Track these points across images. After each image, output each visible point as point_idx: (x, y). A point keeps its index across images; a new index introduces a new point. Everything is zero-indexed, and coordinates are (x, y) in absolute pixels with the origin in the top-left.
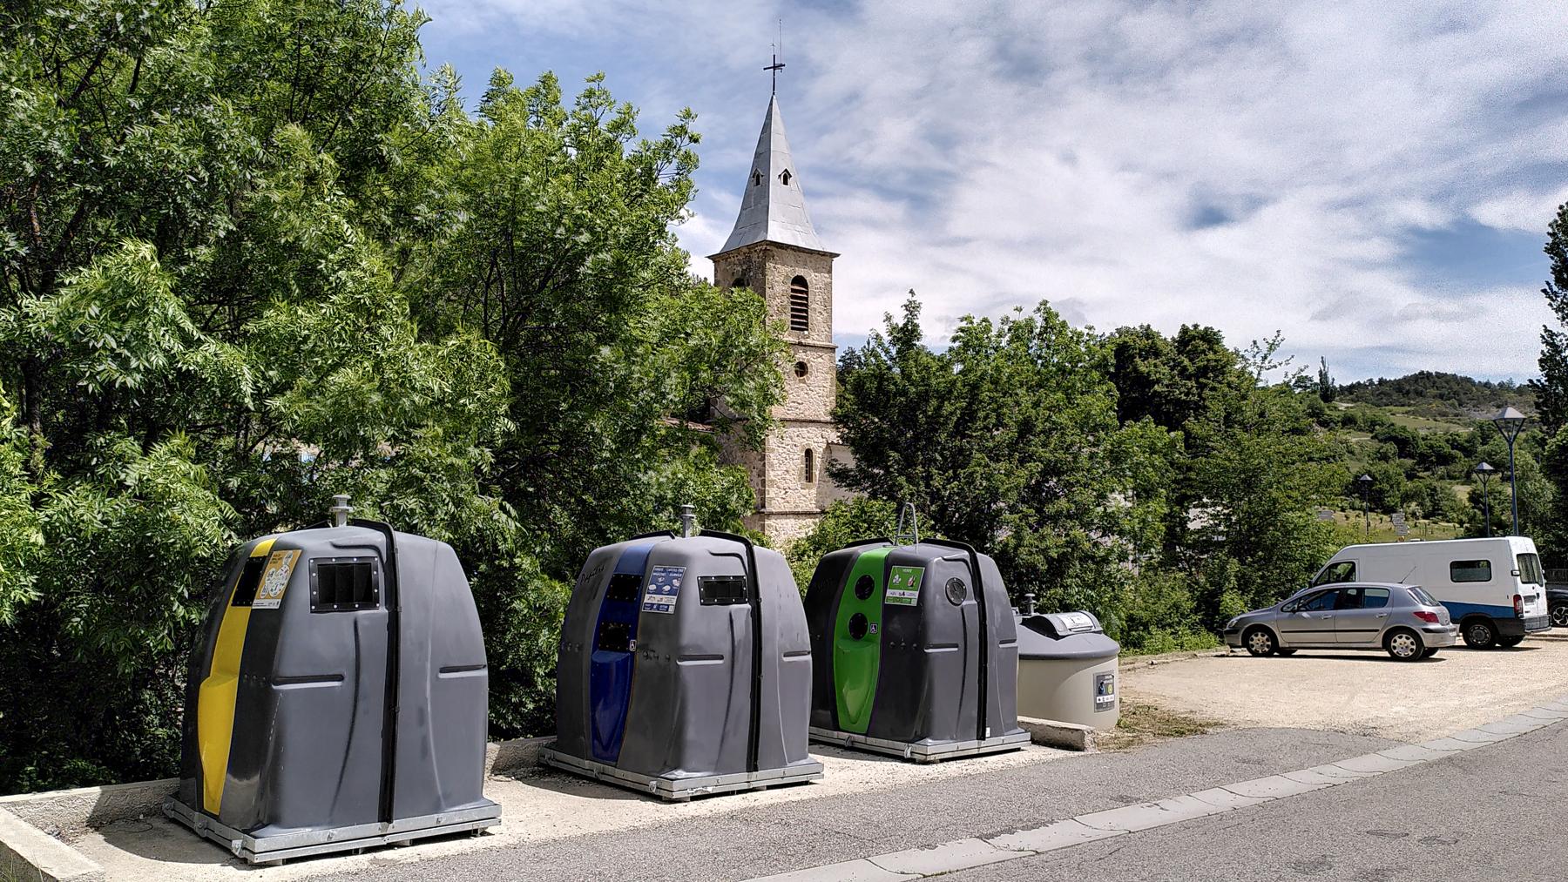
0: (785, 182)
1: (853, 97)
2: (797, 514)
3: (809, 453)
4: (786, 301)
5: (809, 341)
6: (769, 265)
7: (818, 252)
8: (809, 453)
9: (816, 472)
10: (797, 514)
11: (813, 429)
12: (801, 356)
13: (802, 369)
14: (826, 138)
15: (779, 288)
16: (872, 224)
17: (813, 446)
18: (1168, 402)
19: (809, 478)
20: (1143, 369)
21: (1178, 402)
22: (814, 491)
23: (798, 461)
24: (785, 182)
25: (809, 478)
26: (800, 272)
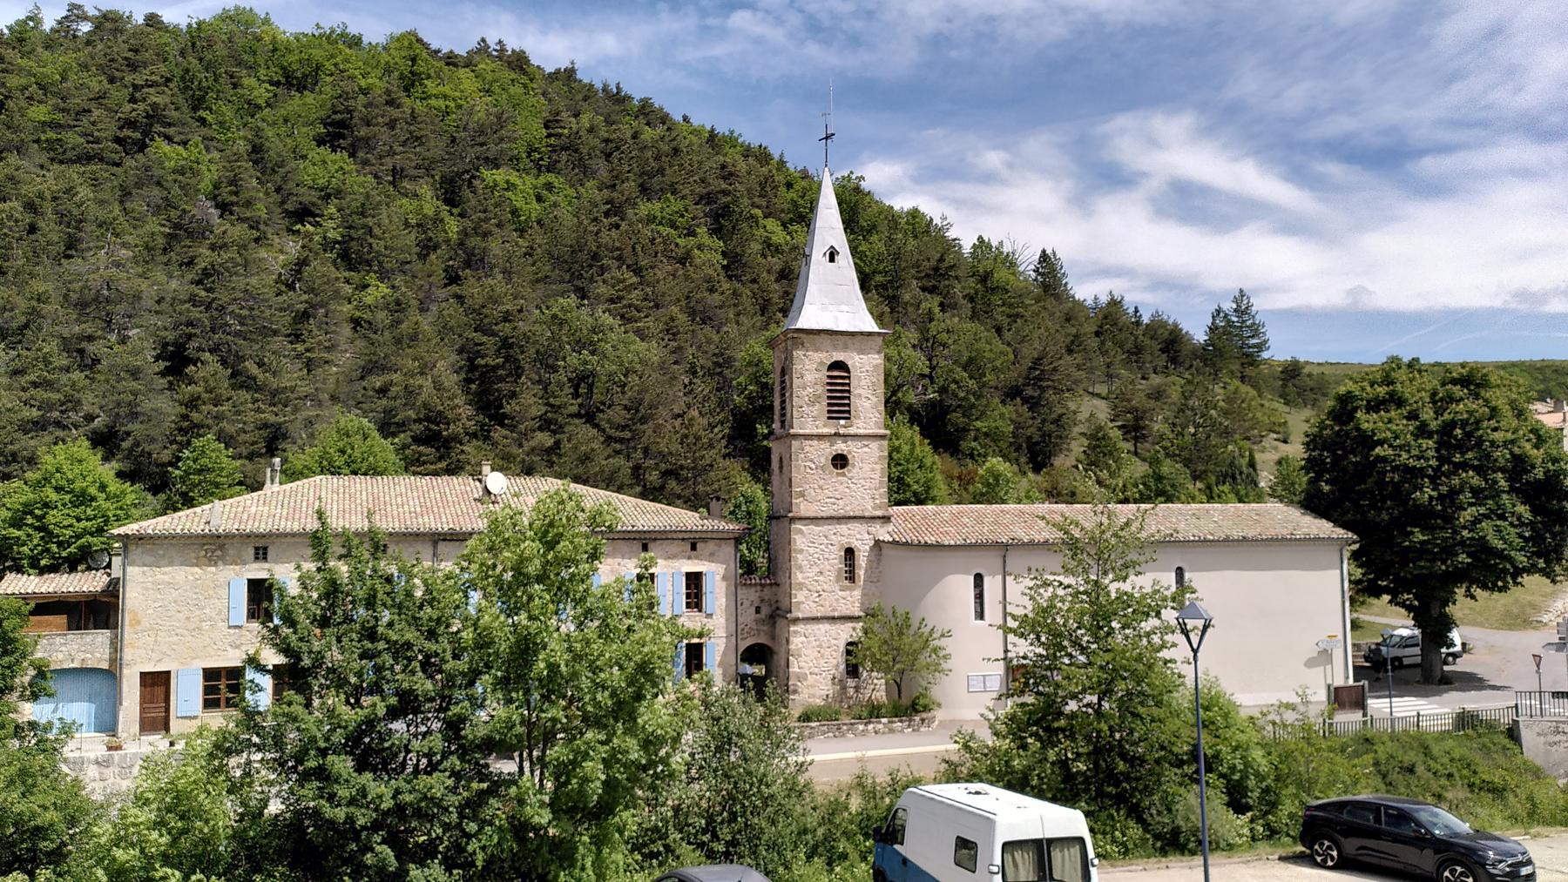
0: (832, 259)
1: (1496, 32)
2: (833, 619)
3: (850, 552)
4: (821, 390)
5: (852, 431)
6: (798, 353)
7: (862, 333)
8: (850, 552)
9: (861, 573)
10: (833, 619)
11: (856, 527)
12: (841, 447)
13: (840, 461)
14: (1456, 87)
15: (809, 377)
16: (1525, 174)
17: (855, 544)
18: (1395, 469)
19: (851, 576)
20: (1365, 426)
21: (1407, 469)
22: (857, 593)
23: (837, 555)
24: (832, 259)
25: (851, 576)
26: (839, 356)
